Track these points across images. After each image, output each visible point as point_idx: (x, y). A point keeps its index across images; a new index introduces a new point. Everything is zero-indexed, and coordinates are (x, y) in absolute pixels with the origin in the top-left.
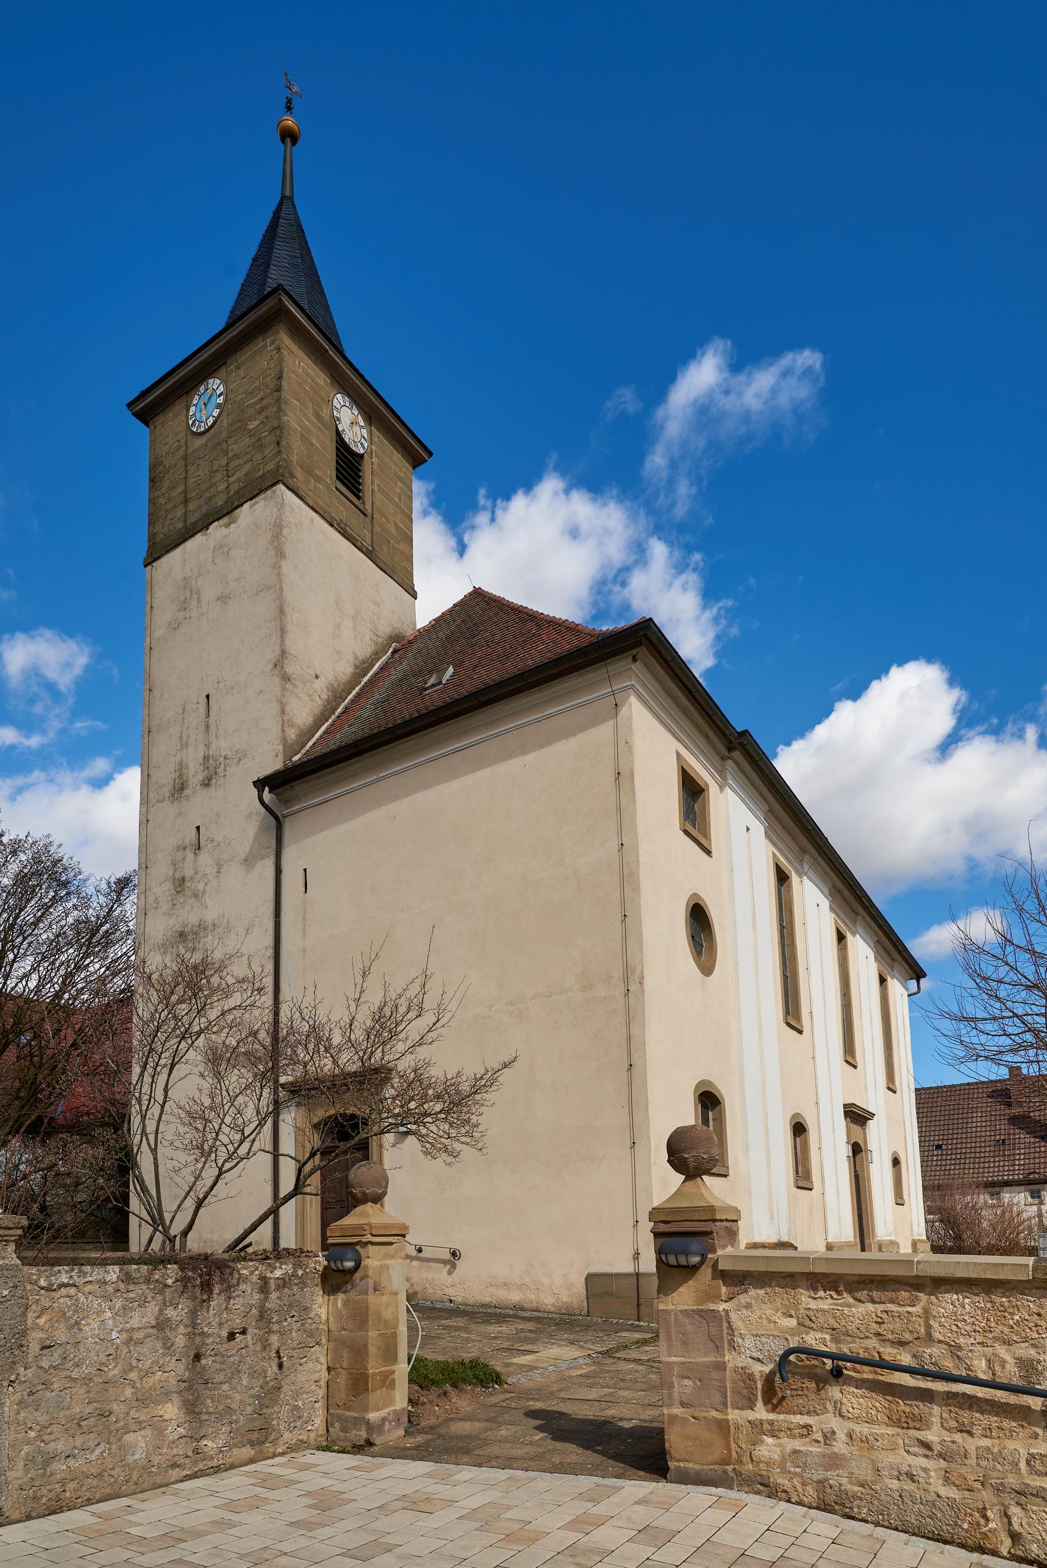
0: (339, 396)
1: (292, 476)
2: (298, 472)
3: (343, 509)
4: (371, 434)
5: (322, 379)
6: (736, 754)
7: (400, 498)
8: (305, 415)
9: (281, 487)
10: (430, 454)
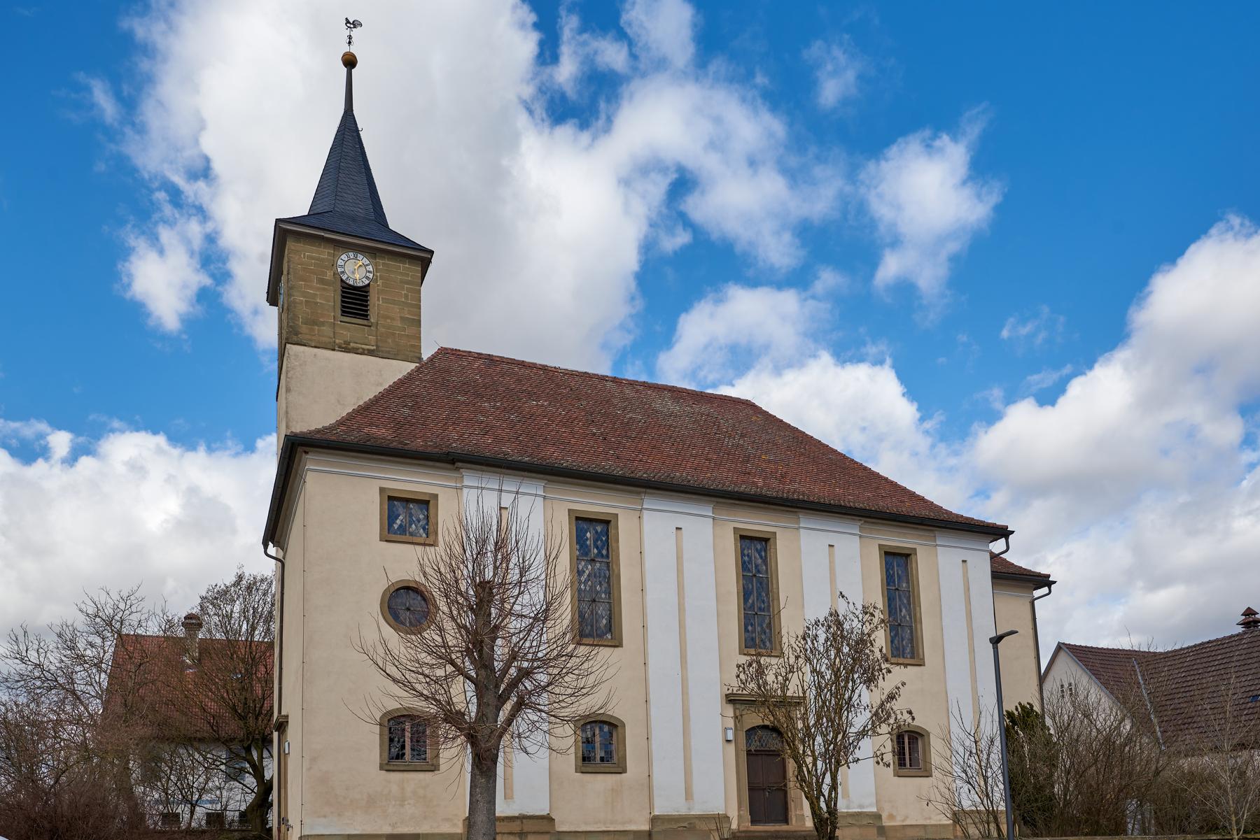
0: (344, 257)
1: (297, 334)
2: (304, 329)
3: (350, 330)
4: (376, 266)
5: (324, 253)
6: (460, 464)
7: (406, 296)
8: (311, 288)
9: (288, 346)
10: (432, 252)
